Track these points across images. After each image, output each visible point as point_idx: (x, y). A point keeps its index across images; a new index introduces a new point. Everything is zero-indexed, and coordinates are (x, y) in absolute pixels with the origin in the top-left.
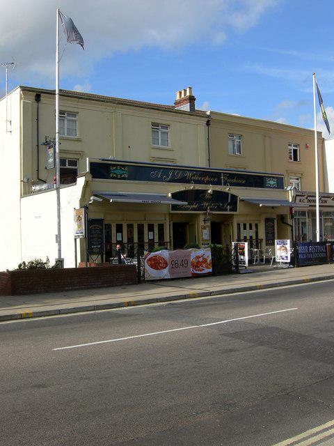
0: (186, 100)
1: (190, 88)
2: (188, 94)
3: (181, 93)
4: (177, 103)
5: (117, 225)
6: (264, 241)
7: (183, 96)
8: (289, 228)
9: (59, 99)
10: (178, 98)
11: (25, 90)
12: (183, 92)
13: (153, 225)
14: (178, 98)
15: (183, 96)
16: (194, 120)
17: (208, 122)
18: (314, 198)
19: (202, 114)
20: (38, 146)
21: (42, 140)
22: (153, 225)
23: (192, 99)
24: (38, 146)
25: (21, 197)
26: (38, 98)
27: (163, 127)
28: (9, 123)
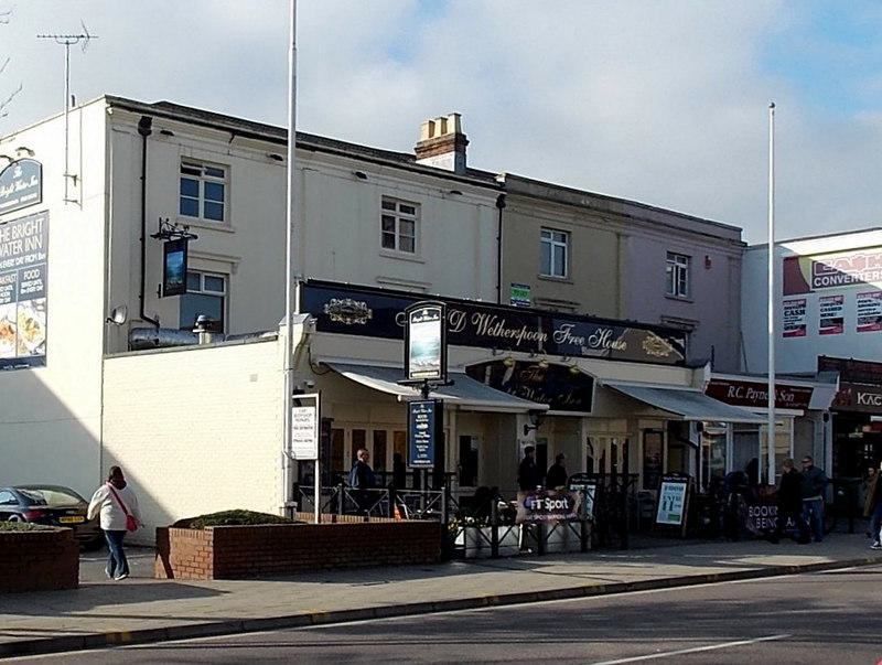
0: (446, 143)
1: (457, 116)
2: (451, 129)
3: (432, 124)
4: (424, 150)
5: (354, 431)
6: (641, 479)
7: (438, 133)
8: (692, 452)
9: (295, 155)
10: (425, 137)
11: (114, 102)
12: (438, 123)
13: (342, 431)
14: (425, 137)
15: (438, 133)
16: (471, 195)
17: (501, 199)
18: (779, 382)
19: (483, 179)
20: (143, 239)
21: (152, 229)
22: (342, 431)
23: (460, 142)
24: (143, 239)
25: (104, 358)
26: (145, 128)
27: (210, 172)
28: (71, 180)
